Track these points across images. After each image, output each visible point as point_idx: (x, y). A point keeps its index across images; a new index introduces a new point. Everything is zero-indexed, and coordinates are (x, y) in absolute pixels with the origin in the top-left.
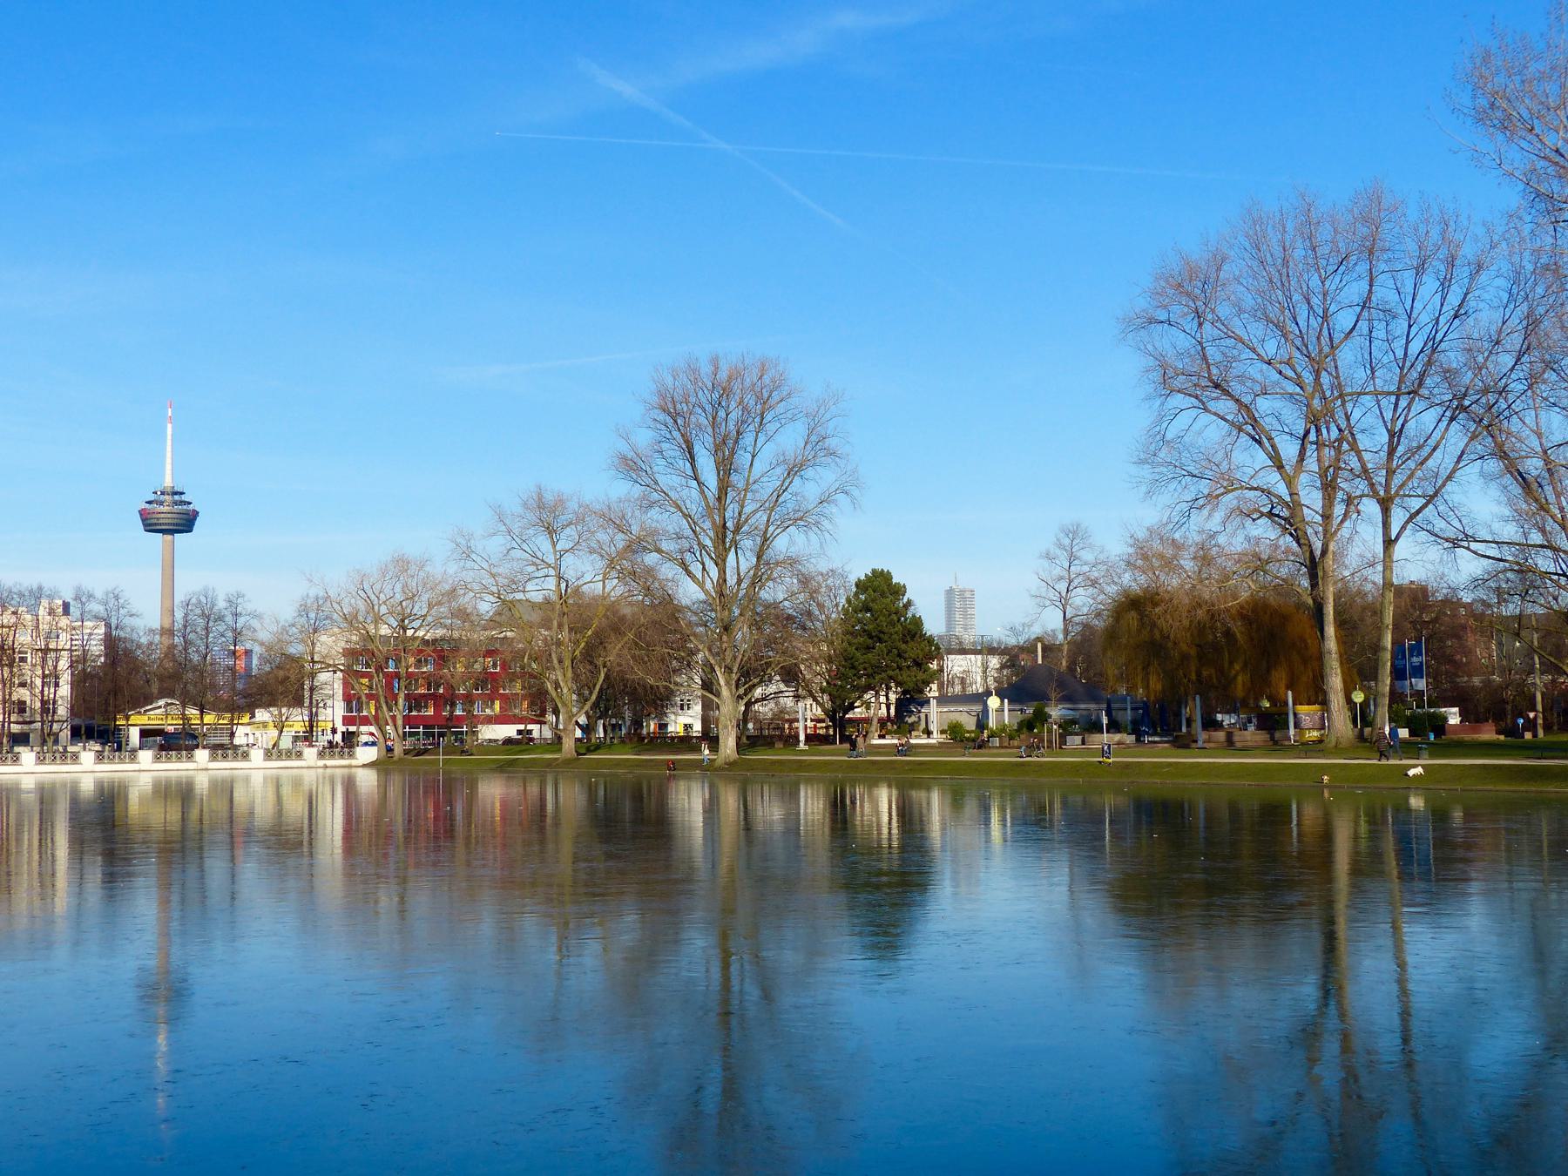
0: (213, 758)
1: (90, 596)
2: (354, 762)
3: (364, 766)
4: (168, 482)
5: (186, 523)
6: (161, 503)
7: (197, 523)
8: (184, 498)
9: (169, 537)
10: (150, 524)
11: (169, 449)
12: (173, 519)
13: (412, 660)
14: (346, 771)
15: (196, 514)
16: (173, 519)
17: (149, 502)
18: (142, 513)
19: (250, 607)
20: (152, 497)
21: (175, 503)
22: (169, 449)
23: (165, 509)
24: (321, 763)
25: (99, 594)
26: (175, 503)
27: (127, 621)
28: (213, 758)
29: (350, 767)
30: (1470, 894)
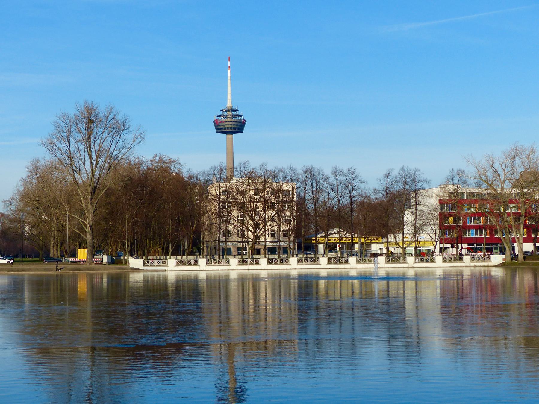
0: (388, 261)
1: (341, 172)
2: (490, 264)
3: (496, 266)
4: (229, 104)
5: (239, 127)
6: (226, 116)
7: (245, 127)
8: (238, 113)
9: (230, 136)
10: (220, 129)
11: (229, 85)
12: (232, 125)
13: (252, 192)
14: (486, 268)
15: (245, 122)
16: (232, 125)
17: (219, 116)
18: (215, 122)
19: (423, 177)
20: (220, 113)
21: (234, 116)
22: (229, 85)
23: (228, 120)
24: (473, 264)
25: (345, 171)
26: (234, 116)
27: (362, 186)
28: (388, 261)
29: (488, 266)
30: (443, 255)
